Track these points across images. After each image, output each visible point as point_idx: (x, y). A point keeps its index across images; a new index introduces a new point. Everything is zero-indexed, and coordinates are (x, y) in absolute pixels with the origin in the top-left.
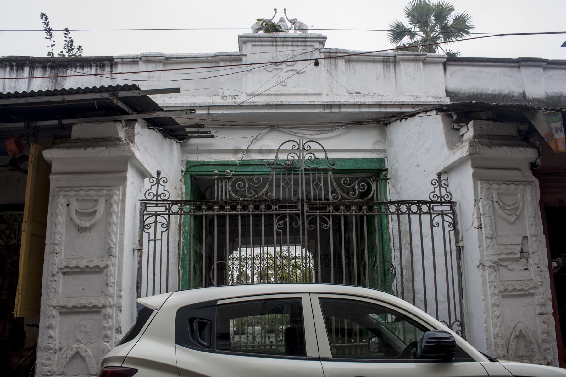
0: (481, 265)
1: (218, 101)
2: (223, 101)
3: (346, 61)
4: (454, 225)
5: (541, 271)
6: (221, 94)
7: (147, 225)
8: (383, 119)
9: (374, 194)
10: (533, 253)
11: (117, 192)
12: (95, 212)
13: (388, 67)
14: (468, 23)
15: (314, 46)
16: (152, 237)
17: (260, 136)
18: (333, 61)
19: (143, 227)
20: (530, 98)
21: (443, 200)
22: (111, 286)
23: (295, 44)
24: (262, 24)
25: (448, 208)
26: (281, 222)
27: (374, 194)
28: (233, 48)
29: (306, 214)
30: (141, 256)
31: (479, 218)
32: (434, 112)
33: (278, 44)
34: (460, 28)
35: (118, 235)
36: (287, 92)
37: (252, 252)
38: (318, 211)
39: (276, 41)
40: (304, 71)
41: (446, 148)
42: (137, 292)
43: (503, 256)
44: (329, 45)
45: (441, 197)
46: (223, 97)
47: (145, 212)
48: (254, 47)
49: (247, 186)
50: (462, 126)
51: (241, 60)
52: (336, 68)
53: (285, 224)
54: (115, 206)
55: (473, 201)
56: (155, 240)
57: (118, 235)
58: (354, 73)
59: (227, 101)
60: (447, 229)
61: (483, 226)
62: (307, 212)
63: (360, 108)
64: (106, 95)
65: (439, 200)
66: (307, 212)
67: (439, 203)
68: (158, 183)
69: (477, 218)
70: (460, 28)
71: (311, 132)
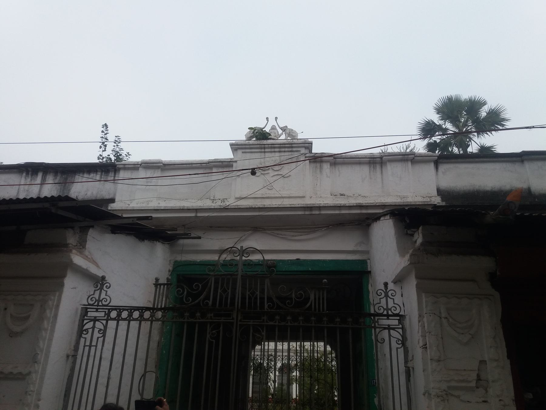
0: (427, 393)
1: (208, 204)
2: (213, 205)
3: (331, 165)
4: (404, 342)
5: (504, 406)
6: (212, 198)
7: (85, 330)
8: (361, 220)
9: (311, 303)
10: (493, 381)
11: (52, 298)
12: (27, 318)
13: (375, 168)
14: (503, 116)
15: (300, 151)
16: (88, 343)
17: (244, 238)
18: (318, 165)
19: (81, 331)
20: (537, 194)
21: (390, 313)
22: (30, 395)
23: (282, 150)
24: (253, 132)
25: (396, 322)
26: (214, 332)
27: (311, 303)
28: (227, 154)
29: (239, 323)
30: (74, 363)
31: (424, 336)
32: (388, 217)
33: (266, 150)
34: (494, 121)
35: (46, 341)
36: (273, 196)
37: (276, 346)
38: (252, 321)
39: (265, 148)
40: (290, 176)
41: (398, 255)
42: (64, 400)
43: (453, 384)
44: (316, 149)
45: (387, 309)
46: (213, 200)
47: (86, 317)
48: (244, 154)
49: (185, 293)
50: (415, 232)
51: (232, 166)
52: (321, 172)
53: (218, 333)
54: (48, 311)
55: (417, 316)
56: (90, 346)
57: (46, 341)
58: (339, 176)
59: (217, 204)
60: (394, 345)
61: (428, 346)
62: (240, 321)
63: (340, 210)
64: (47, 205)
65: (385, 313)
66: (240, 321)
67: (385, 315)
68: (101, 289)
69: (422, 336)
70: (494, 121)
71: (292, 234)
